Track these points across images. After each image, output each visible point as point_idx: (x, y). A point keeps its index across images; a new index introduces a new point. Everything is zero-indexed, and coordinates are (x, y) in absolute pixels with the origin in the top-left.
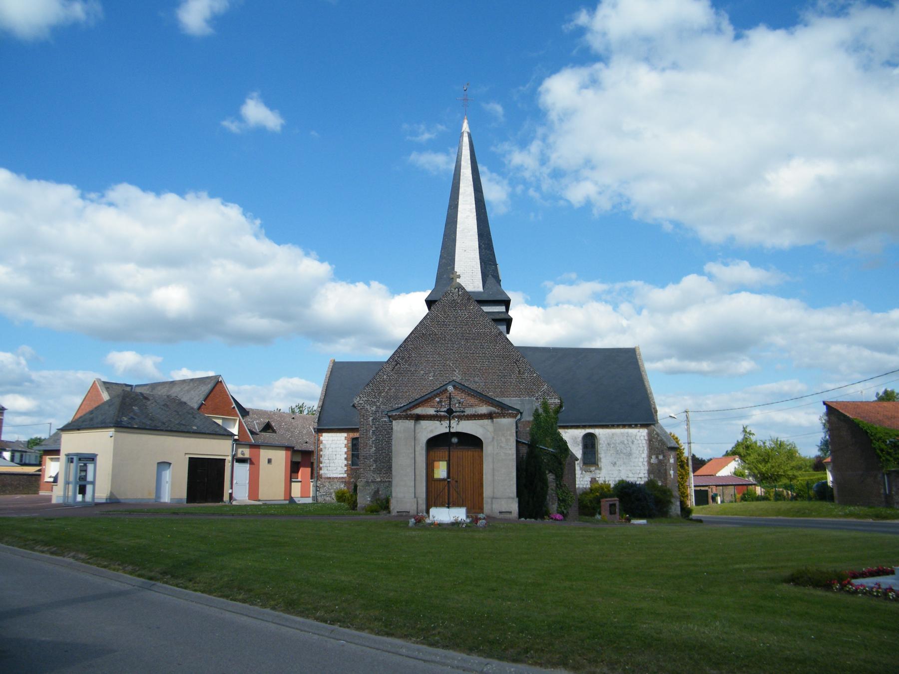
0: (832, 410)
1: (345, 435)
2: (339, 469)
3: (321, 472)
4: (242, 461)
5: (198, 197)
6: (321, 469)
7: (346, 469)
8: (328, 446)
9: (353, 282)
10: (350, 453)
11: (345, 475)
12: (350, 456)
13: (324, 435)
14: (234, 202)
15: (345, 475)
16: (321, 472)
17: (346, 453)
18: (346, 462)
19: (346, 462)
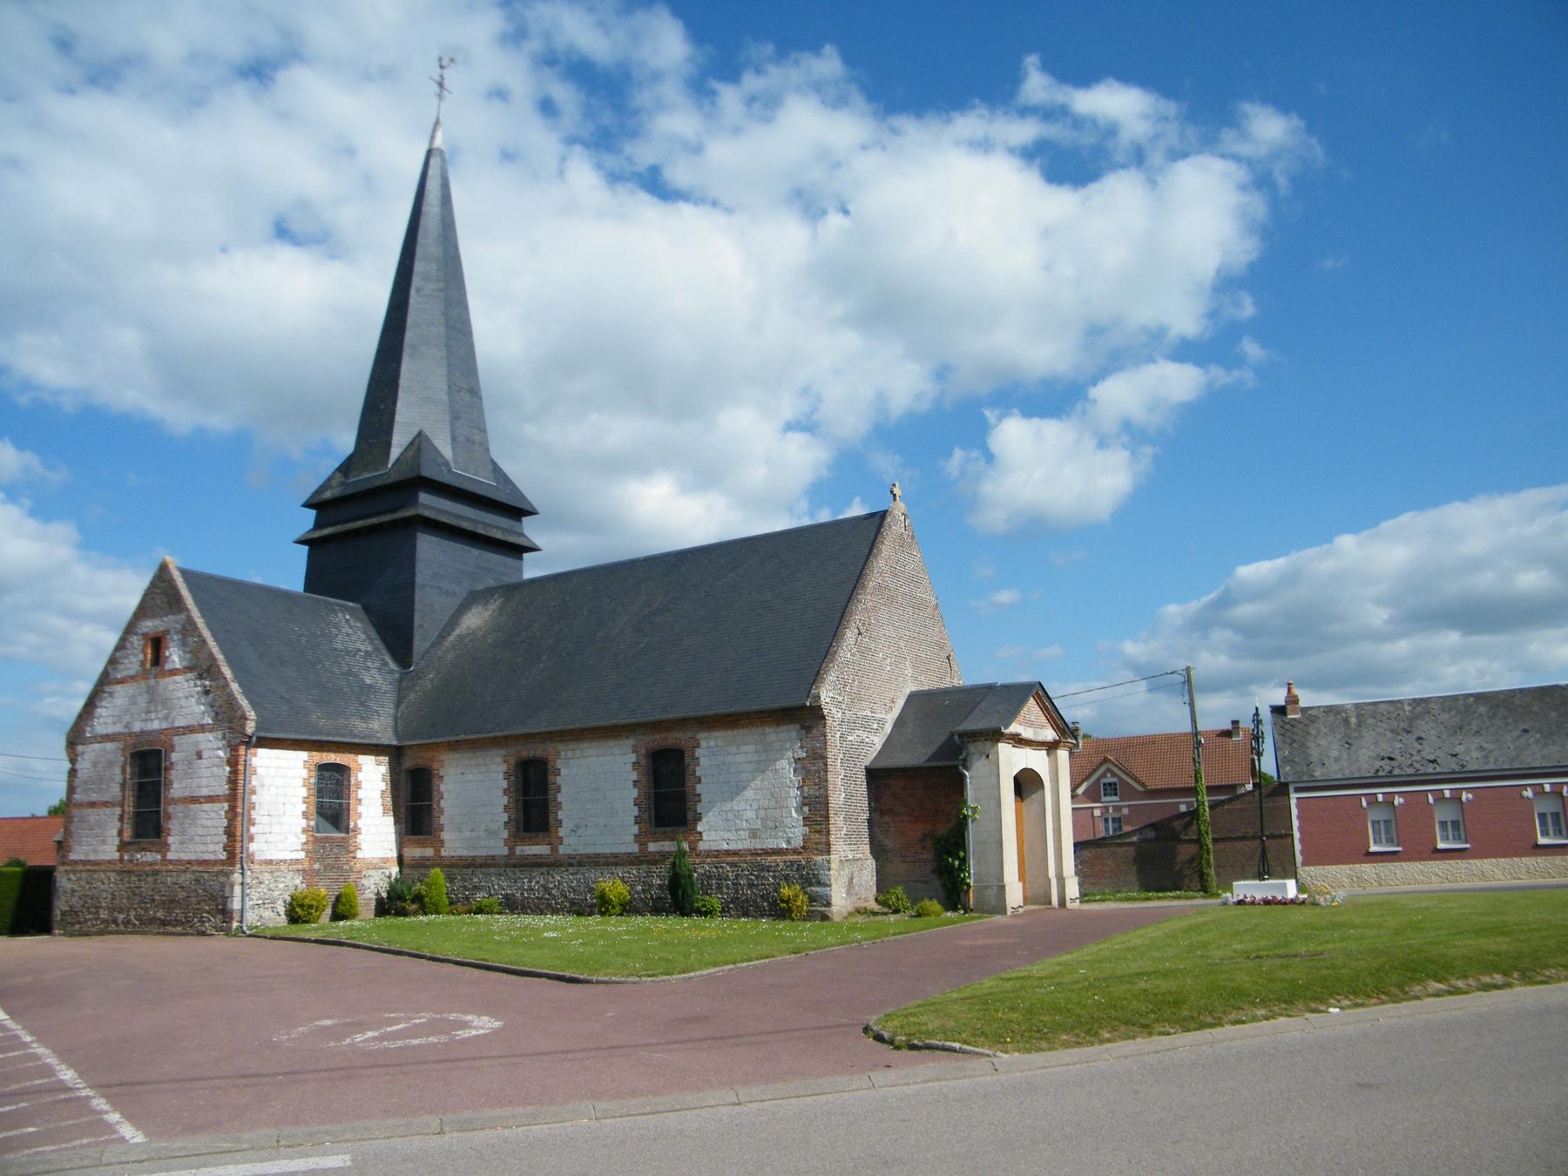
0: (420, 434)
1: (629, 743)
2: (292, 839)
3: (253, 847)
4: (669, 798)
5: (894, 131)
6: (251, 839)
7: (303, 838)
8: (268, 781)
9: (1375, 524)
10: (313, 799)
11: (302, 855)
12: (313, 809)
13: (262, 752)
14: (794, 40)
15: (302, 855)
16: (253, 847)
17: (559, 790)
18: (304, 823)
19: (304, 823)
